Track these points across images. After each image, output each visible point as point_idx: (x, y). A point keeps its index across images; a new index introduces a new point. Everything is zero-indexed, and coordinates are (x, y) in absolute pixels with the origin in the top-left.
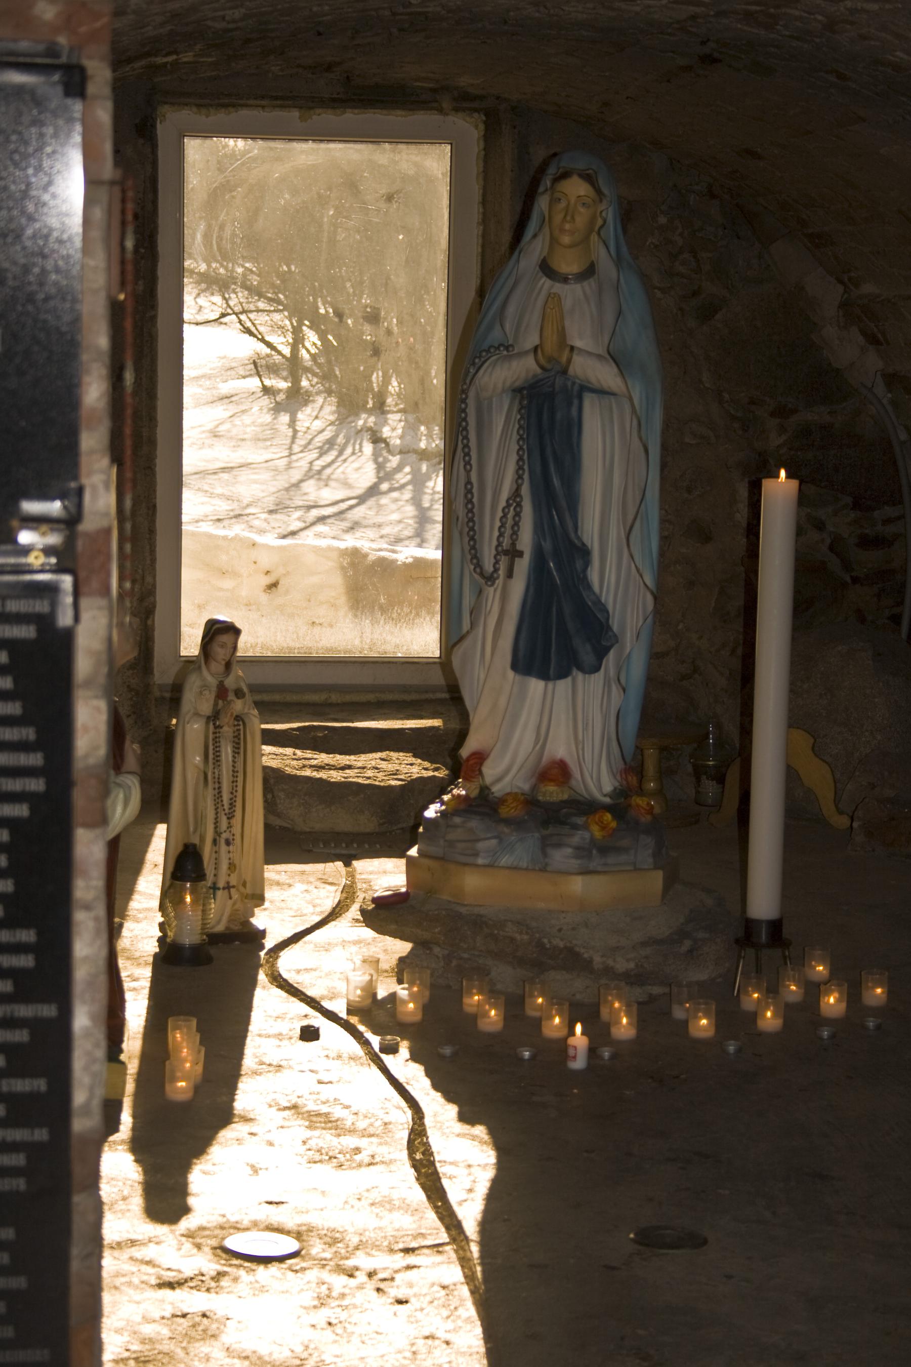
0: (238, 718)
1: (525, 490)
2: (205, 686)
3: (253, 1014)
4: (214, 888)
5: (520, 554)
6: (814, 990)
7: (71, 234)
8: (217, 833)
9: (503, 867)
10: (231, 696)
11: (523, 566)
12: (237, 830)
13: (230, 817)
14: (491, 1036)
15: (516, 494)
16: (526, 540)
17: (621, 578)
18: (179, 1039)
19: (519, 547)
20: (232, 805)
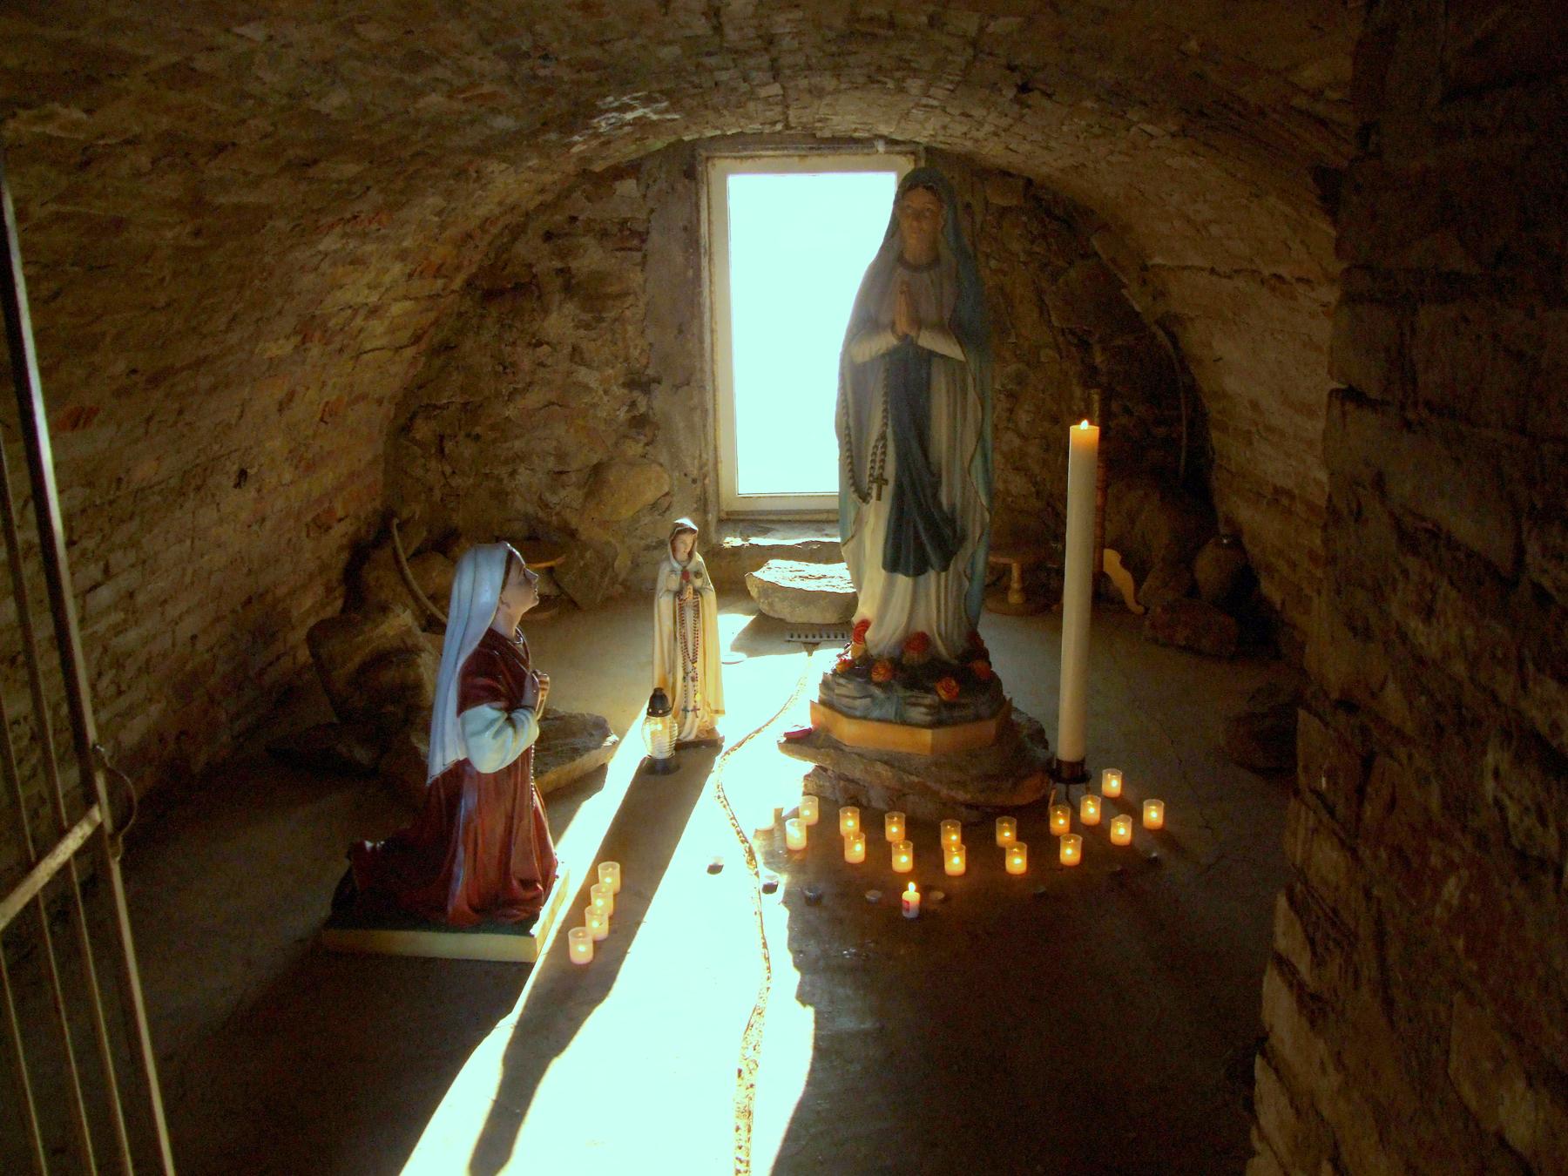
0: (697, 592)
1: (889, 431)
2: (673, 571)
3: (493, 1096)
4: (685, 710)
5: (886, 482)
6: (1114, 806)
7: (571, 298)
8: (686, 673)
9: (1102, 556)
10: (692, 577)
11: (888, 491)
12: (699, 670)
13: (694, 661)
14: (853, 866)
15: (883, 437)
16: (890, 471)
17: (967, 489)
18: (912, 886)
19: (886, 476)
20: (695, 654)
